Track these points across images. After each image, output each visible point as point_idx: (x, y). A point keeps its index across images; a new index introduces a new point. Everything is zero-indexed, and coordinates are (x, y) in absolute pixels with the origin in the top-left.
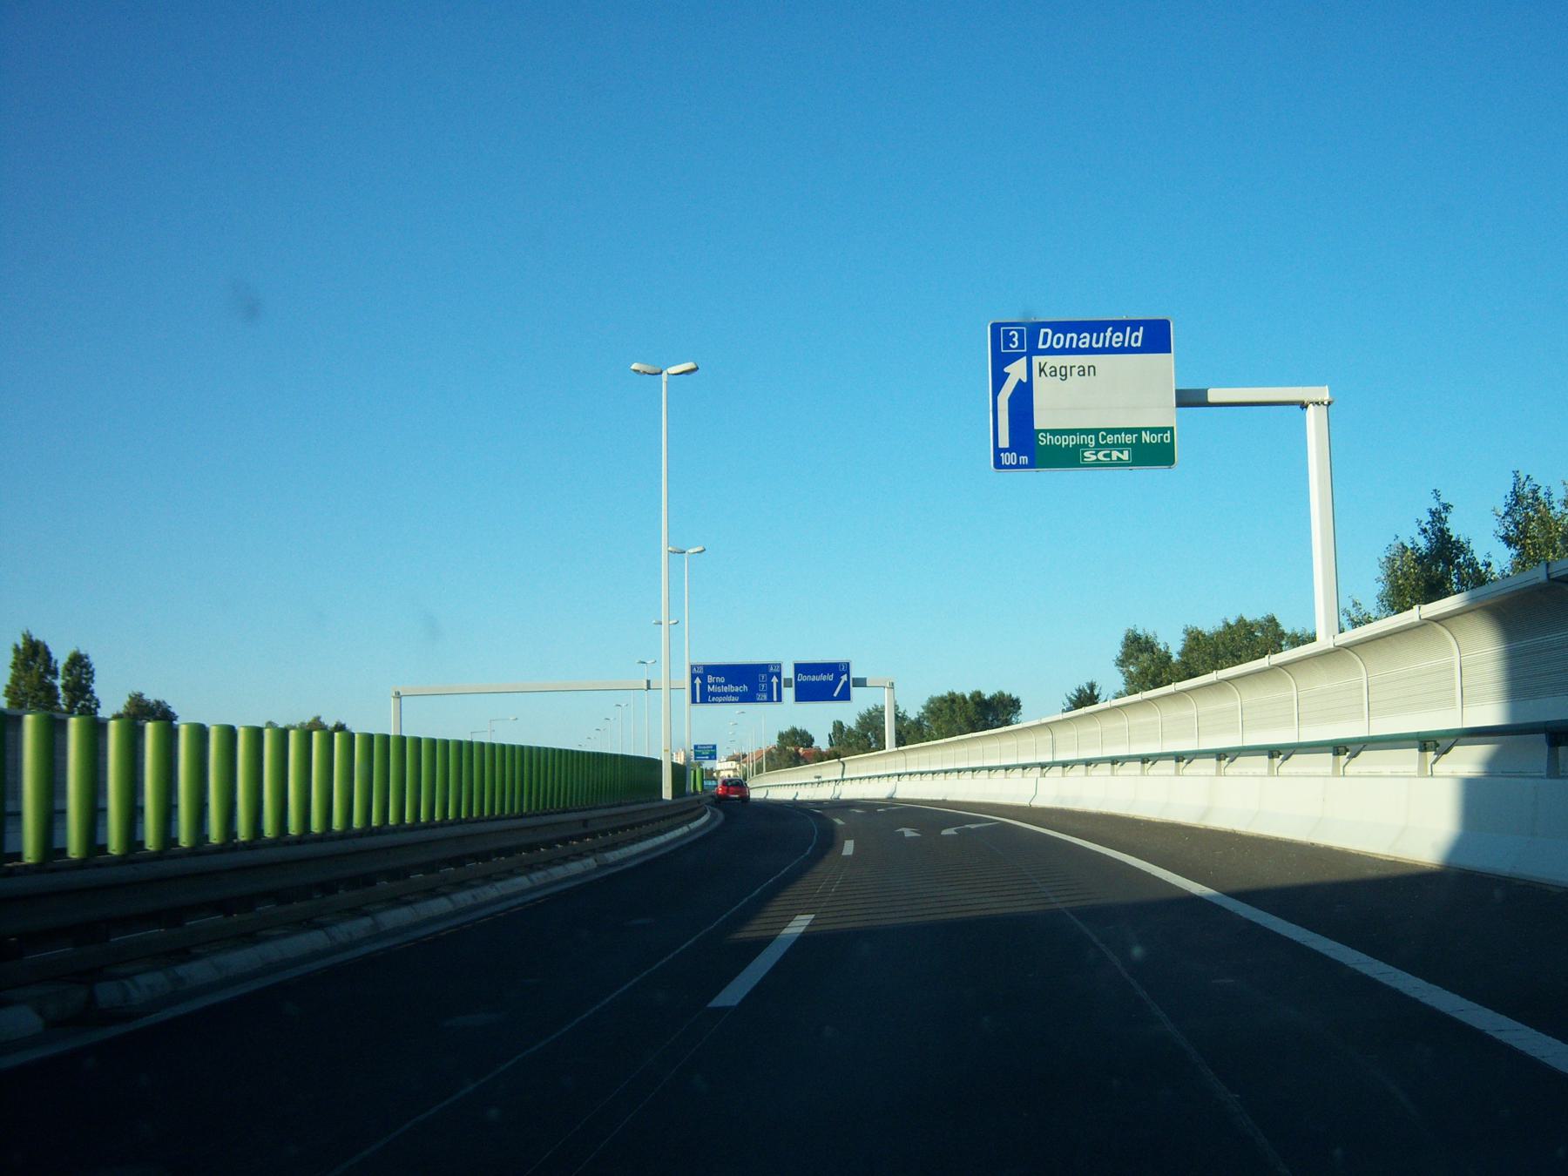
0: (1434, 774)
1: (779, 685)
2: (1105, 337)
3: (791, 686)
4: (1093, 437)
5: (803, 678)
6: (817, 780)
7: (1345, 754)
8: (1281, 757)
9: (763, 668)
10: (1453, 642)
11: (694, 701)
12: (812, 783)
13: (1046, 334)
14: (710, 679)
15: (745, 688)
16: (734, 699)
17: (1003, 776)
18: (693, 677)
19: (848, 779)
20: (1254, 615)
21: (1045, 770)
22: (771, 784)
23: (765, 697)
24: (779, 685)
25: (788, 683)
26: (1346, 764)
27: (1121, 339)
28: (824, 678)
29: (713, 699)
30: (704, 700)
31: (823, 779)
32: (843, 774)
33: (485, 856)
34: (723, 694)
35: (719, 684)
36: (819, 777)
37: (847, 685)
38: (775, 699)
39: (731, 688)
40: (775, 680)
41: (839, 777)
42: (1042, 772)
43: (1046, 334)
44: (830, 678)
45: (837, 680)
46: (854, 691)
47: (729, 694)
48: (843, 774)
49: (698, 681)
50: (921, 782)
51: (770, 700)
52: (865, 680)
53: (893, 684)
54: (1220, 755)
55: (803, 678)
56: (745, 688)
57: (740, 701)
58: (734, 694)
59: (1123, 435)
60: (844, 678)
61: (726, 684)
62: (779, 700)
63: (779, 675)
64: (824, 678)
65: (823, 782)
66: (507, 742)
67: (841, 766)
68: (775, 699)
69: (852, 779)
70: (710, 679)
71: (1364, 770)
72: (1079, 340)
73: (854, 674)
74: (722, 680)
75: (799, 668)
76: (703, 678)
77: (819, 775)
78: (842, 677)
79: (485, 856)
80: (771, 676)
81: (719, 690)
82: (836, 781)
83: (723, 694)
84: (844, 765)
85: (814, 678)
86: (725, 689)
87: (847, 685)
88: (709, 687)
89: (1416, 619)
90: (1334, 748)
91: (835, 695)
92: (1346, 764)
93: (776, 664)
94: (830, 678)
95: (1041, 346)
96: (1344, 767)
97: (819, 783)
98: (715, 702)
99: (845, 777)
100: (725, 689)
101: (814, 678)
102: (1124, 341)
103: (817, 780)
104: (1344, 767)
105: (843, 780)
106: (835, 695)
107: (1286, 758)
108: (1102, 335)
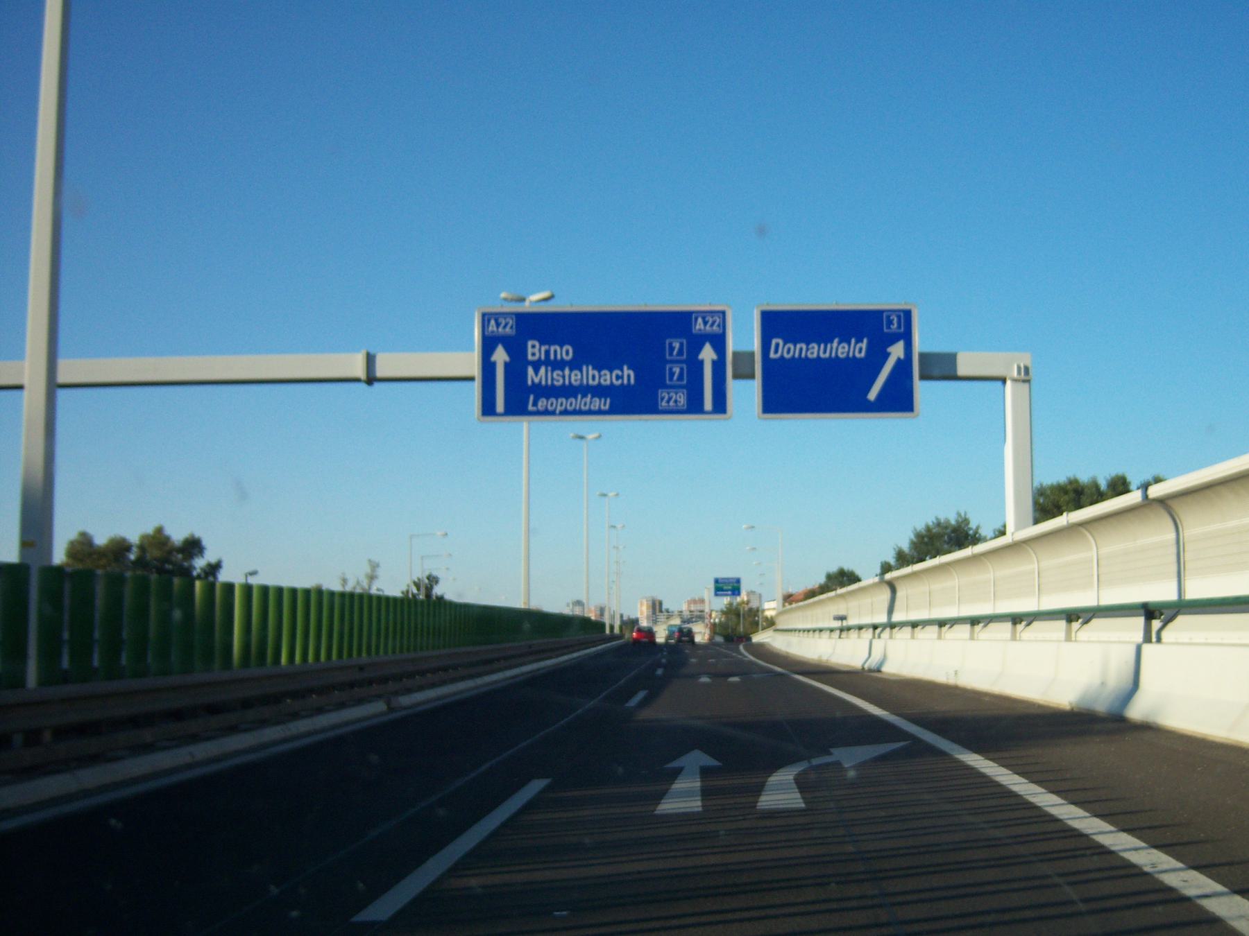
0: (980, 638)
1: (719, 367)
2: (832, 348)
3: (752, 376)
4: (591, 382)
5: (783, 350)
6: (837, 624)
7: (1077, 621)
8: (1080, 621)
9: (679, 322)
10: (1093, 542)
11: (488, 408)
12: (832, 630)
13: (777, 345)
14: (534, 350)
15: (628, 375)
16: (597, 403)
17: (909, 636)
18: (489, 345)
19: (902, 625)
20: (950, 516)
21: (1156, 624)
22: (809, 626)
23: (682, 398)
24: (719, 367)
25: (743, 359)
26: (1078, 630)
27: (846, 349)
28: (840, 349)
29: (542, 403)
30: (516, 407)
31: (852, 621)
32: (891, 611)
33: (423, 673)
34: (568, 391)
35: (558, 365)
36: (842, 618)
37: (903, 367)
38: (708, 404)
39: (589, 375)
40: (707, 354)
41: (882, 618)
42: (874, 633)
43: (777, 345)
44: (859, 349)
45: (878, 355)
46: (923, 390)
47: (585, 390)
48: (891, 611)
49: (500, 356)
50: (1016, 645)
51: (694, 406)
52: (951, 359)
53: (1027, 370)
54: (1071, 616)
55: (783, 350)
56: (628, 375)
57: (613, 411)
58: (599, 391)
59: (567, 371)
60: (897, 351)
61: (575, 365)
62: (720, 405)
63: (719, 342)
64: (840, 349)
65: (849, 629)
66: (286, 583)
67: (885, 594)
68: (708, 404)
69: (914, 625)
70: (534, 350)
71: (1184, 637)
72: (807, 350)
73: (920, 344)
74: (565, 352)
75: (775, 323)
76: (516, 348)
77: (842, 613)
78: (890, 349)
79: (423, 673)
80: (696, 343)
81: (557, 378)
82: (875, 627)
83: (568, 391)
84: (894, 591)
85: (815, 351)
86: (575, 378)
87: (903, 367)
88: (530, 371)
89: (1065, 523)
90: (1068, 615)
91: (872, 395)
92: (1078, 630)
93: (712, 313)
94: (859, 349)
95: (530, 408)
96: (1020, 633)
97: (842, 630)
98: (546, 412)
99: (897, 617)
100: (575, 378)
101: (815, 351)
102: (848, 352)
103: (837, 624)
104: (1020, 633)
105: (892, 626)
106: (872, 395)
107: (1029, 624)
108: (829, 346)
